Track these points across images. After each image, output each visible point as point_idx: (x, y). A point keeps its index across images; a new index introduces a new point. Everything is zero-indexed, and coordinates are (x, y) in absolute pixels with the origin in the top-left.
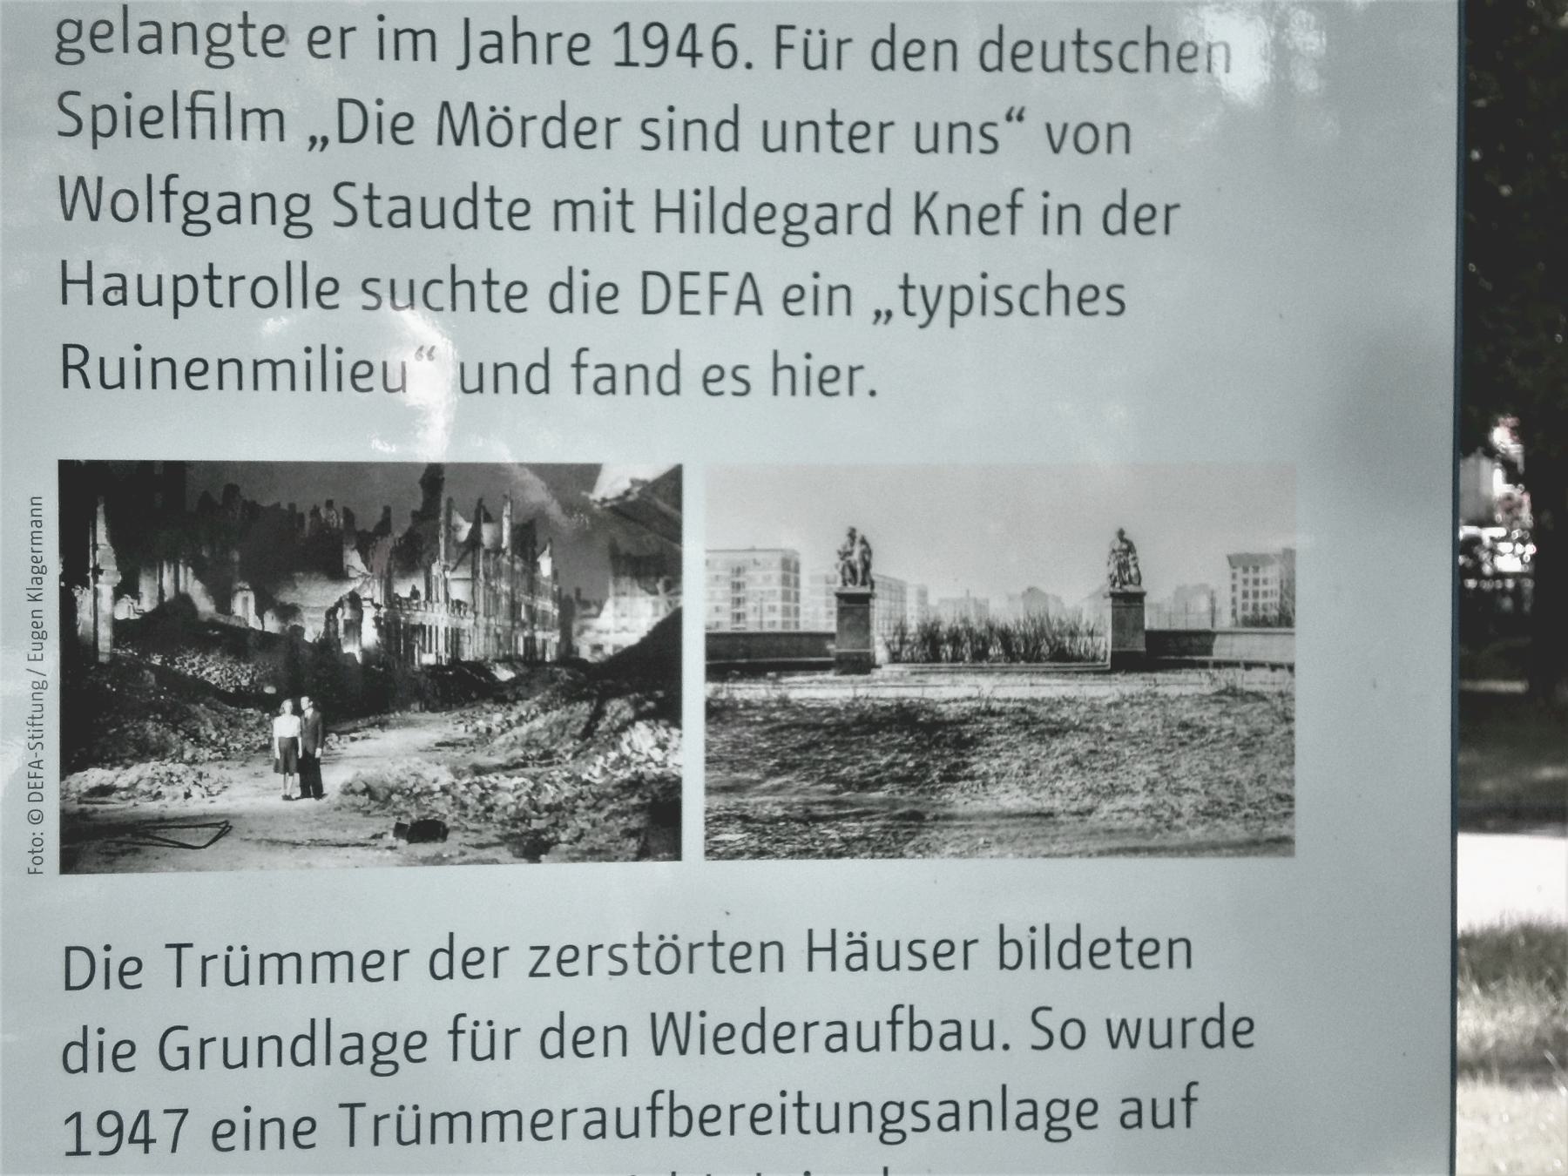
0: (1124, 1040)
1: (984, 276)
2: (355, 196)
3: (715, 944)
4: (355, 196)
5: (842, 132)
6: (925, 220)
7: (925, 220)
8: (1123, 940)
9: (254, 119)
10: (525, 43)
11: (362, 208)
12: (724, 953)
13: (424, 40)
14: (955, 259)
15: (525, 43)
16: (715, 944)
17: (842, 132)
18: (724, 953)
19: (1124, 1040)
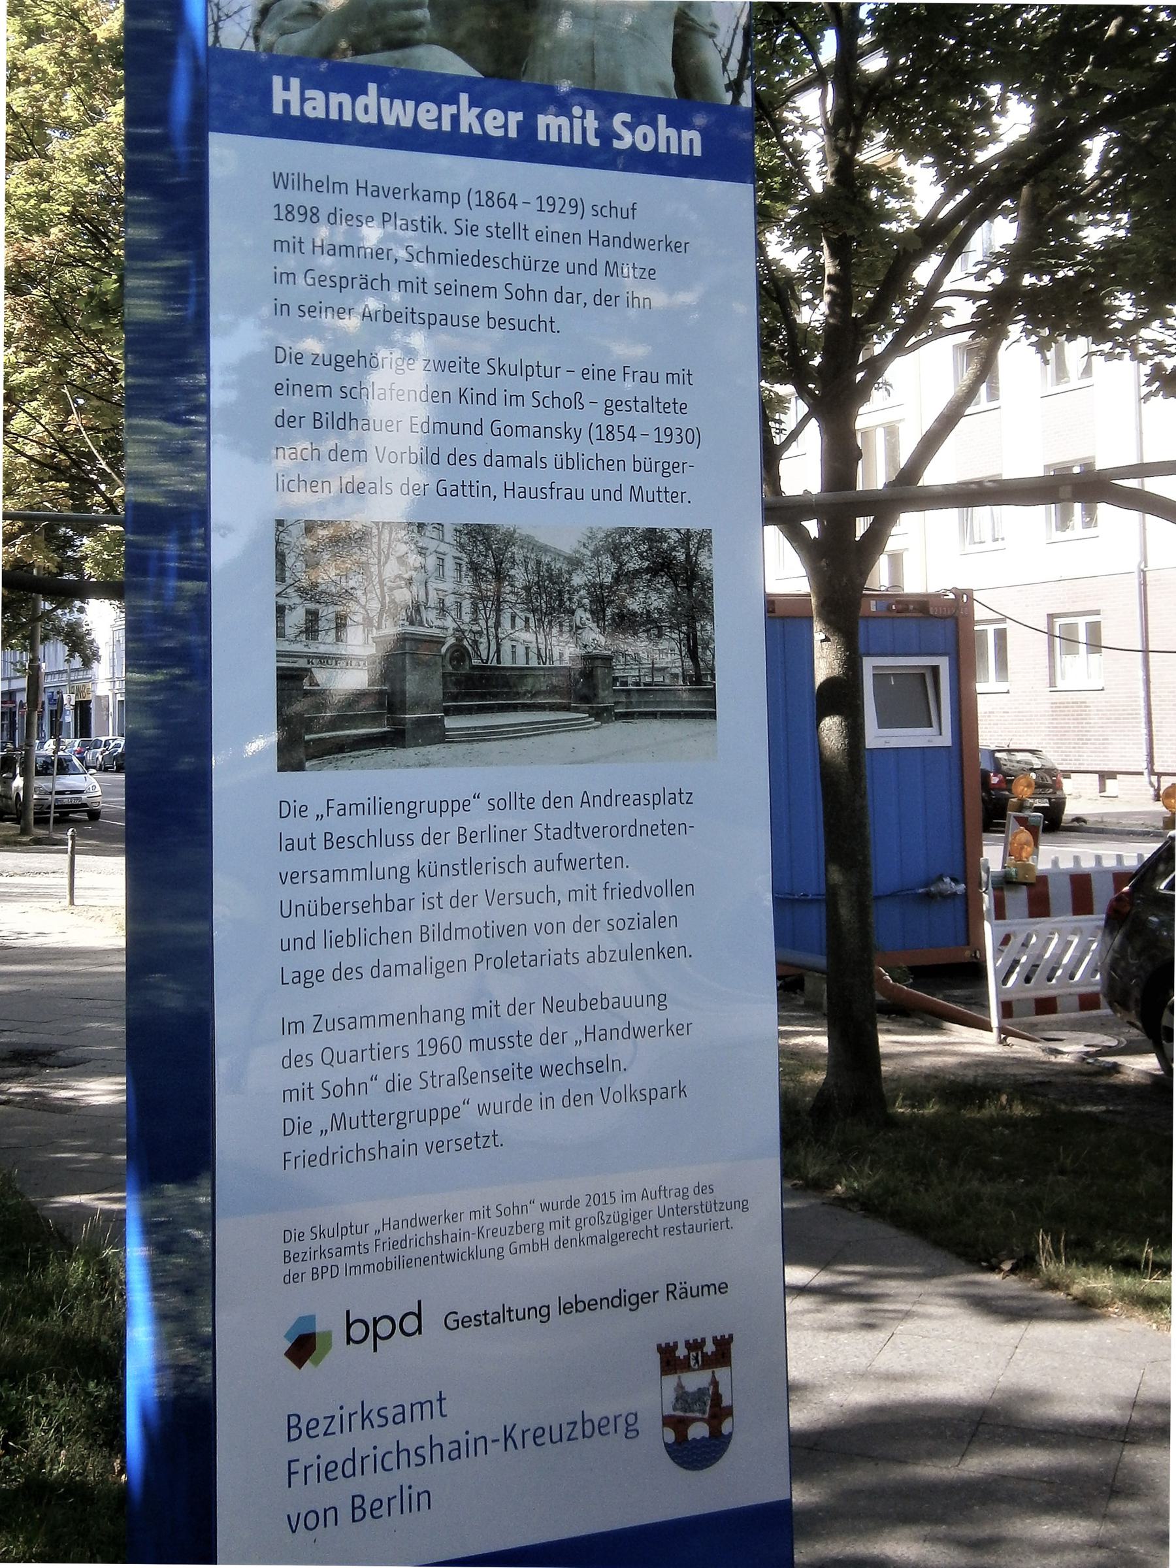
0: (281, 183)
1: (467, 1433)
2: (541, 829)
3: (599, 858)
4: (541, 829)
5: (522, 1071)
6: (510, 1441)
7: (510, 1441)
8: (663, 825)
9: (337, 186)
10: (531, 293)
11: (544, 832)
12: (602, 861)
13: (343, 186)
14: (450, 1228)
15: (531, 293)
16: (599, 858)
17: (522, 1071)
18: (602, 861)
19: (281, 183)
